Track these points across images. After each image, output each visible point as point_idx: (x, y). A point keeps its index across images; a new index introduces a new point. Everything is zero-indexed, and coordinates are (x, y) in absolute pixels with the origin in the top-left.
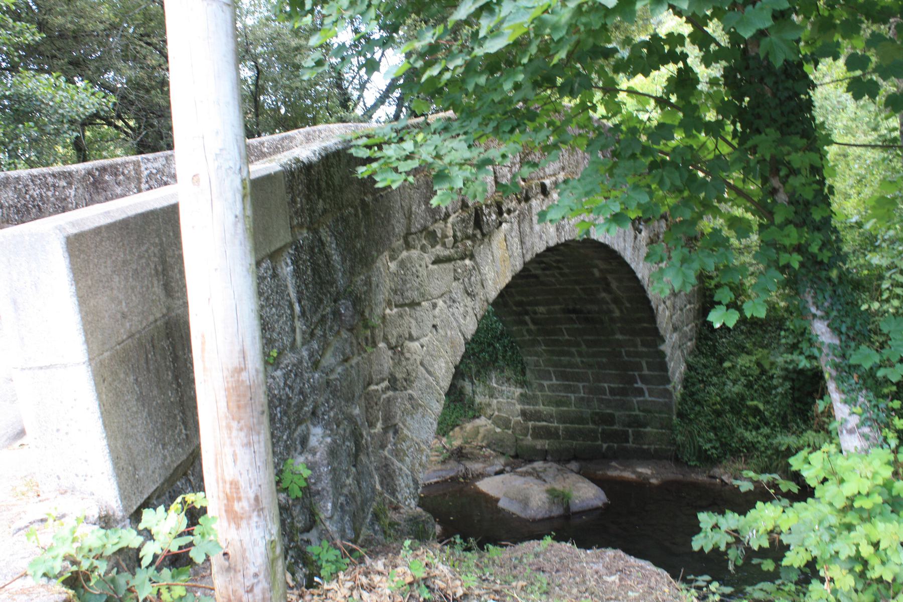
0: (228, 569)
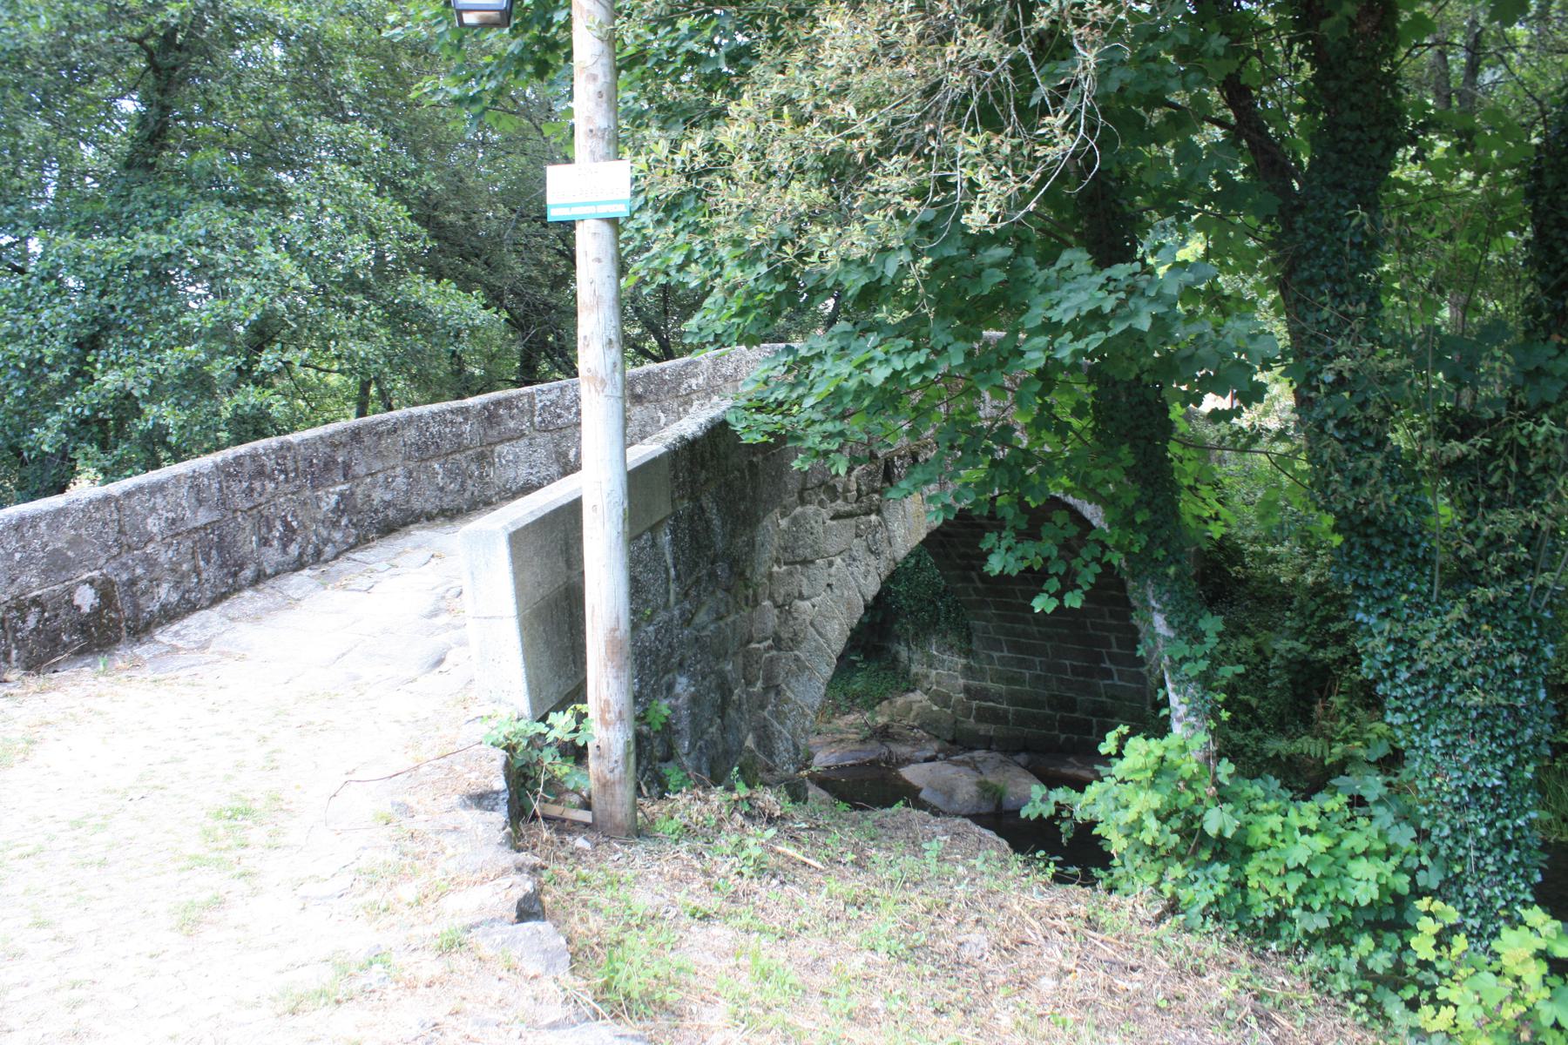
0: (599, 756)
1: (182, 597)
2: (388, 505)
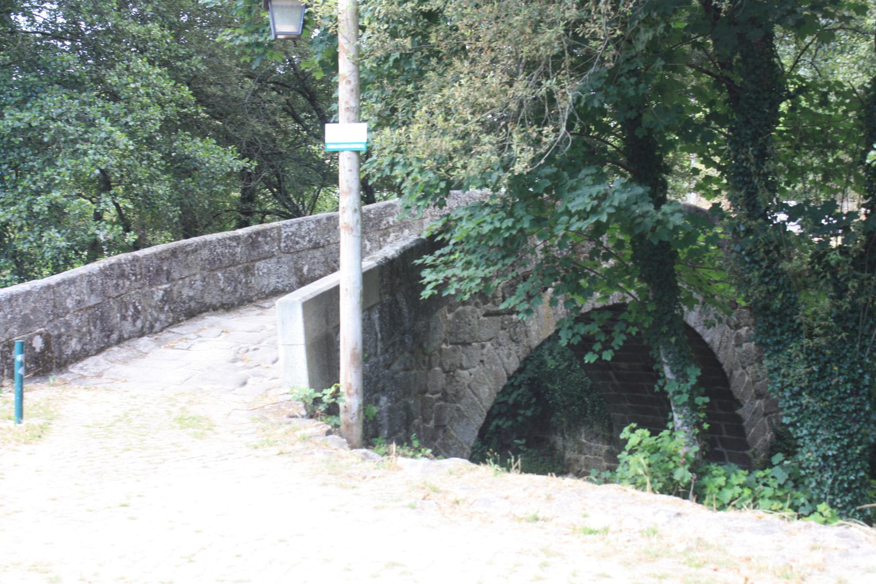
1: (82, 348)
2: (191, 298)
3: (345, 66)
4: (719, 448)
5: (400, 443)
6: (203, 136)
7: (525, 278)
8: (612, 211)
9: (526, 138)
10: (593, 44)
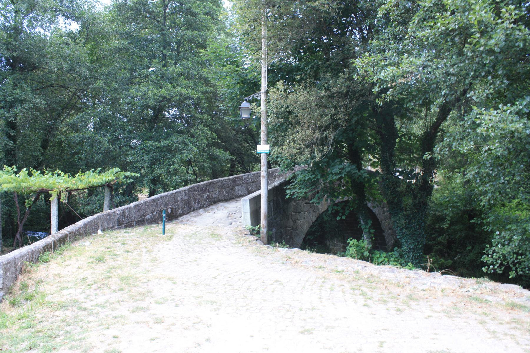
2: (215, 198)
3: (263, 127)
4: (378, 245)
5: (279, 243)
6: (220, 148)
7: (318, 192)
8: (346, 173)
9: (319, 150)
10: (339, 121)
